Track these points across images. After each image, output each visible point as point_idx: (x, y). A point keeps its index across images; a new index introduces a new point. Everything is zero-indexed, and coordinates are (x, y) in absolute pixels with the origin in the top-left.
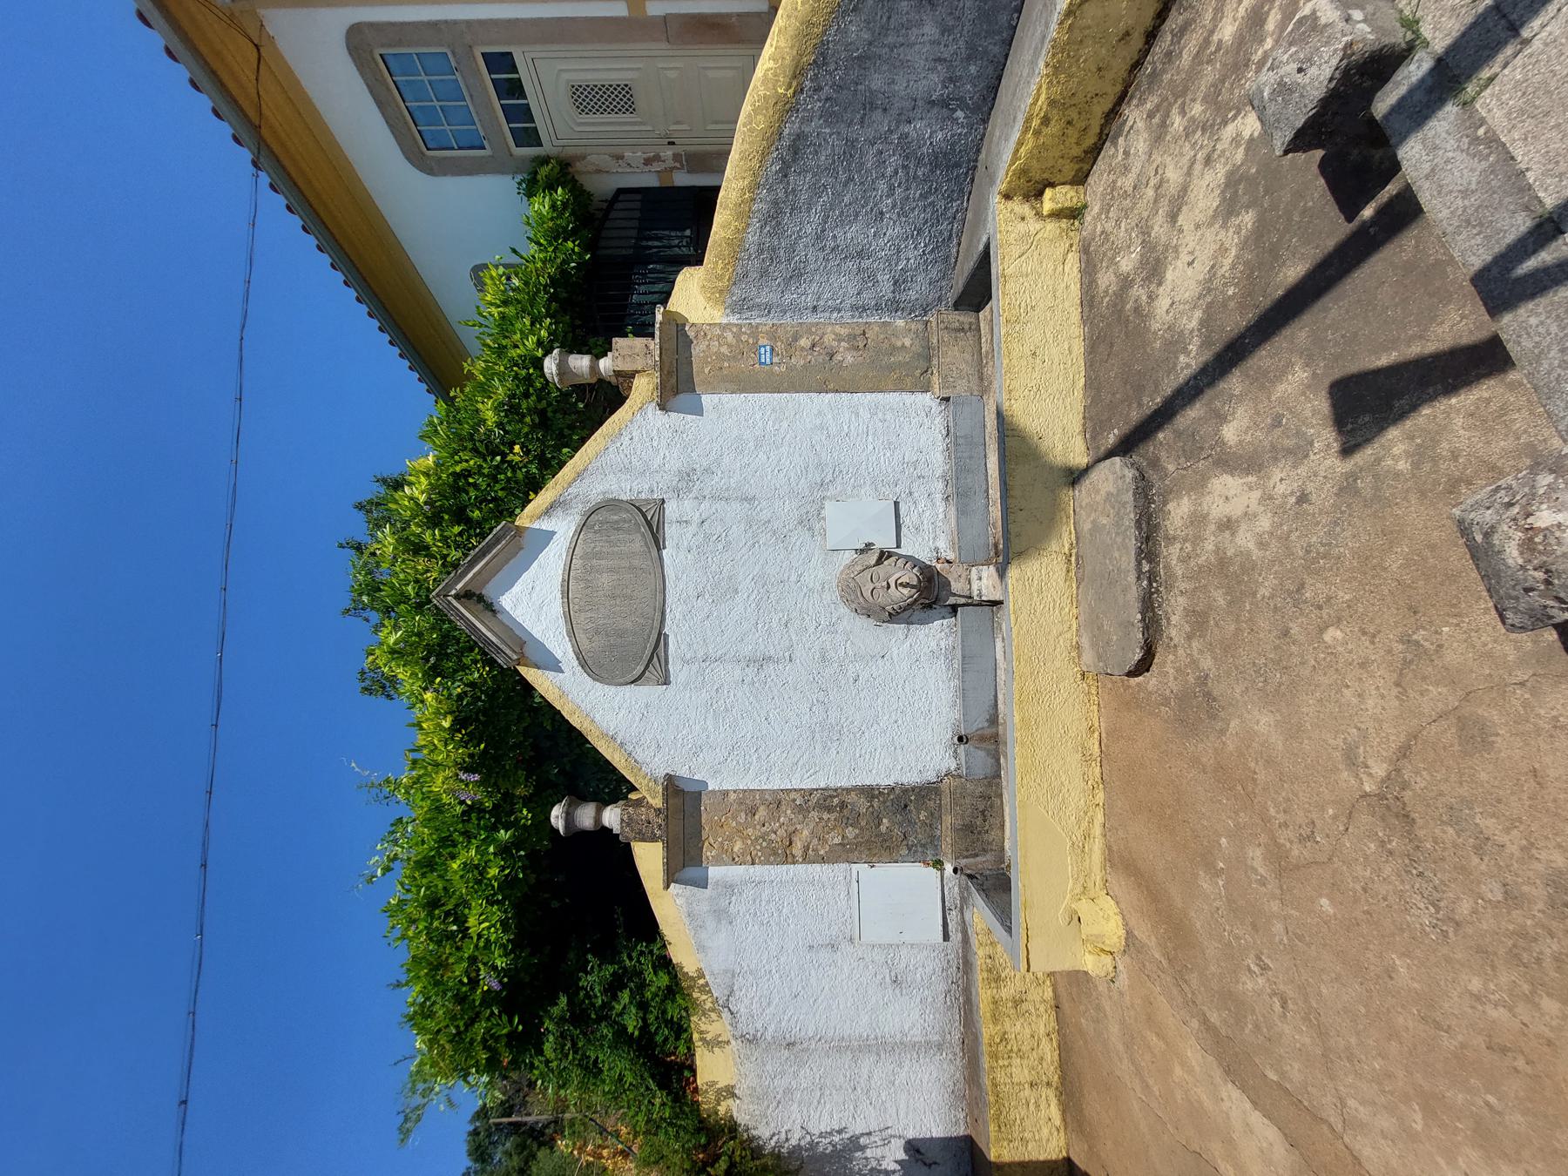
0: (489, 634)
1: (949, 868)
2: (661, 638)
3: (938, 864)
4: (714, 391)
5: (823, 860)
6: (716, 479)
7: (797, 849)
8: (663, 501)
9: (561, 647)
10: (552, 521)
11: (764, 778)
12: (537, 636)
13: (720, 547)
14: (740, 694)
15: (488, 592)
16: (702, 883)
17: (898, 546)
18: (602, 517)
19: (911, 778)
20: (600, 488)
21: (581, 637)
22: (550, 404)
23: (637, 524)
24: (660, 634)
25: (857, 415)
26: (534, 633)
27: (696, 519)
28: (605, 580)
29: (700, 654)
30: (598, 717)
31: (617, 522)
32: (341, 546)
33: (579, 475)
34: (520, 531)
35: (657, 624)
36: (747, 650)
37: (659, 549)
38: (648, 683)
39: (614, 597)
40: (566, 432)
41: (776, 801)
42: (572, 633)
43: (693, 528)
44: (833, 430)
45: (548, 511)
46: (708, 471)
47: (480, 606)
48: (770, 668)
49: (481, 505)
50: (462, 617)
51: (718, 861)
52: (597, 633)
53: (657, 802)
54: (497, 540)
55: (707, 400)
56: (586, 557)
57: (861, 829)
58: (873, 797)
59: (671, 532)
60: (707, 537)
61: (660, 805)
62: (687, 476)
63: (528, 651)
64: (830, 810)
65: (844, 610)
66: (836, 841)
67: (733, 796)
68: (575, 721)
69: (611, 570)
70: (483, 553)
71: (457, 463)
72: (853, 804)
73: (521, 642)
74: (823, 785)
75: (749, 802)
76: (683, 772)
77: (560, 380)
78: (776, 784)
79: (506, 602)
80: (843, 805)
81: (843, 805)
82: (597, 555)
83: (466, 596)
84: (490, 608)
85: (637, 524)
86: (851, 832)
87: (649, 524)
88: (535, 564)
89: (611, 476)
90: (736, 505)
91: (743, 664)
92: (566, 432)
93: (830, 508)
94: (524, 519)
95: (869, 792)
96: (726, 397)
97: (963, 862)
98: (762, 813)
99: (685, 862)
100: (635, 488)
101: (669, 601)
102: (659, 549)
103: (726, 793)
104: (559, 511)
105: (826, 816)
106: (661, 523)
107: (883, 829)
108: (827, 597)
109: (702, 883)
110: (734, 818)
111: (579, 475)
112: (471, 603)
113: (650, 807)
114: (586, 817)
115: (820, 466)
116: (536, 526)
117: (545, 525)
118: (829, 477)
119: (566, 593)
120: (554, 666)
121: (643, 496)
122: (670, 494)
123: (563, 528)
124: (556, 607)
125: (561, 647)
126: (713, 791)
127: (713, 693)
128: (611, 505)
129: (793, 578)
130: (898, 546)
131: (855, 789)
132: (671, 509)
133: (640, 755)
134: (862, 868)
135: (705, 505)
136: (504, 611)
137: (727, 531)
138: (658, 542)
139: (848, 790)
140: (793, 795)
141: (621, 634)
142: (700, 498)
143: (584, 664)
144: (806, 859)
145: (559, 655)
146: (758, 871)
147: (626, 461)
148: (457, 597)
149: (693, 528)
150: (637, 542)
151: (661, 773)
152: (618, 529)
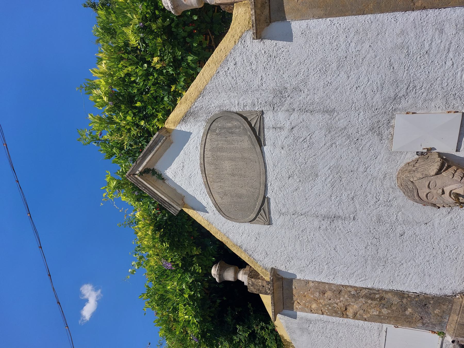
0: (163, 197)
1: (449, 339)
2: (265, 200)
3: (442, 334)
4: (302, 17)
5: (365, 320)
6: (303, 95)
7: (350, 312)
8: (262, 113)
9: (204, 199)
10: (190, 118)
11: (331, 277)
12: (191, 193)
13: (305, 146)
14: (317, 234)
15: (158, 167)
16: (295, 317)
17: (458, 150)
18: (221, 122)
19: (433, 291)
20: (217, 103)
21: (217, 197)
22: (172, 20)
23: (244, 129)
24: (264, 197)
25: (442, 31)
26: (188, 191)
27: (288, 126)
28: (227, 165)
29: (291, 210)
30: (231, 236)
31: (230, 128)
32: (85, 6)
33: (201, 94)
34: (168, 131)
35: (262, 192)
36: (324, 211)
37: (261, 146)
38: (258, 223)
39: (233, 175)
40: (188, 40)
41: (339, 290)
42: (210, 193)
43: (284, 133)
44: (414, 49)
45: (184, 119)
46: (296, 89)
47: (155, 177)
48: (339, 223)
49: (144, 102)
50: (146, 188)
51: (302, 310)
52: (225, 194)
53: (268, 278)
54: (156, 143)
55: (297, 26)
56: (212, 150)
57: (393, 311)
58: (403, 298)
59: (269, 134)
60: (296, 139)
61: (269, 280)
62: (280, 93)
63: (186, 200)
64: (373, 299)
65: (399, 193)
66: (375, 313)
67: (311, 284)
68: (218, 237)
69: (232, 159)
70: (149, 151)
71: (122, 69)
72: (389, 299)
73: (182, 197)
74: (369, 286)
75: (322, 288)
76: (282, 268)
77: (176, 12)
78: (339, 281)
79: (169, 173)
80: (382, 298)
81: (382, 298)
82: (221, 149)
83: (146, 171)
84: (161, 178)
85: (244, 129)
86: (385, 311)
87: (253, 129)
88: (182, 152)
89: (223, 94)
90: (319, 116)
91: (320, 218)
92: (188, 40)
93: (400, 120)
94: (169, 124)
95: (401, 295)
96: (313, 22)
97: (460, 339)
98: (329, 294)
99: (285, 303)
100: (242, 103)
101: (269, 179)
102: (261, 146)
103: (307, 282)
104: (191, 119)
105: (370, 302)
106: (262, 128)
107: (407, 313)
108: (387, 183)
109: (295, 317)
110: (312, 294)
111: (201, 94)
112: (149, 176)
113: (264, 280)
114: (229, 276)
115: (396, 83)
116: (178, 128)
117: (184, 128)
118: (403, 92)
119: (204, 171)
120: (203, 209)
121: (248, 108)
122: (267, 107)
123: (196, 130)
124: (199, 179)
125: (204, 199)
126: (300, 280)
127: (300, 232)
128: (226, 115)
129: (361, 169)
130: (458, 150)
131: (391, 291)
132: (269, 119)
133: (256, 256)
134: (391, 327)
135: (295, 115)
136: (169, 179)
137: (311, 135)
138: (260, 141)
139: (386, 292)
140: (349, 289)
141: (240, 196)
142: (291, 111)
143: (220, 210)
144: (355, 316)
145: (204, 204)
146: (325, 317)
147: (233, 82)
148: (141, 174)
149: (284, 133)
150: (245, 142)
151: (269, 266)
152: (232, 133)
